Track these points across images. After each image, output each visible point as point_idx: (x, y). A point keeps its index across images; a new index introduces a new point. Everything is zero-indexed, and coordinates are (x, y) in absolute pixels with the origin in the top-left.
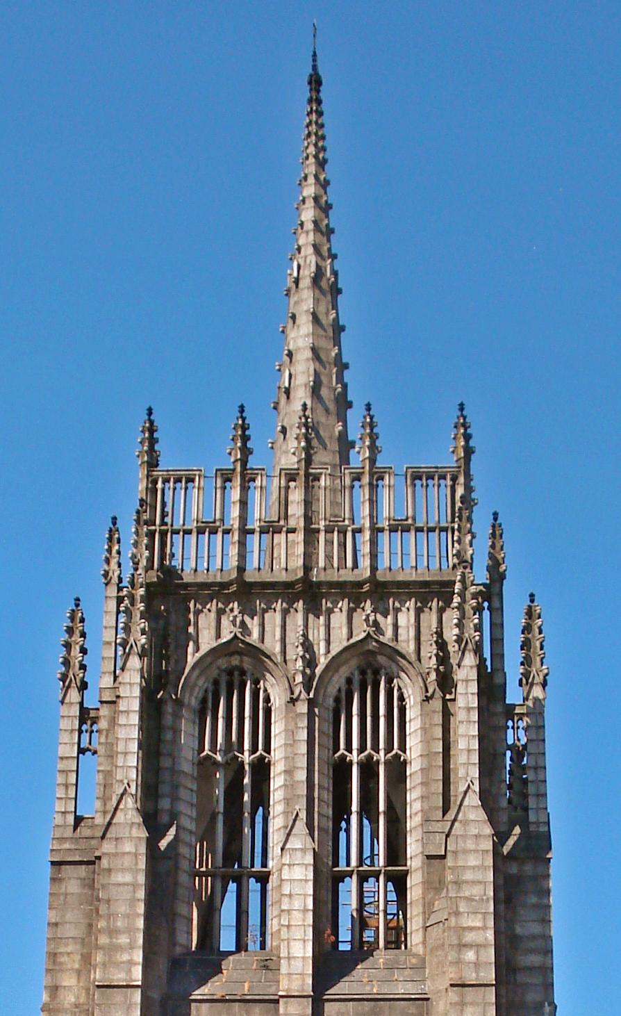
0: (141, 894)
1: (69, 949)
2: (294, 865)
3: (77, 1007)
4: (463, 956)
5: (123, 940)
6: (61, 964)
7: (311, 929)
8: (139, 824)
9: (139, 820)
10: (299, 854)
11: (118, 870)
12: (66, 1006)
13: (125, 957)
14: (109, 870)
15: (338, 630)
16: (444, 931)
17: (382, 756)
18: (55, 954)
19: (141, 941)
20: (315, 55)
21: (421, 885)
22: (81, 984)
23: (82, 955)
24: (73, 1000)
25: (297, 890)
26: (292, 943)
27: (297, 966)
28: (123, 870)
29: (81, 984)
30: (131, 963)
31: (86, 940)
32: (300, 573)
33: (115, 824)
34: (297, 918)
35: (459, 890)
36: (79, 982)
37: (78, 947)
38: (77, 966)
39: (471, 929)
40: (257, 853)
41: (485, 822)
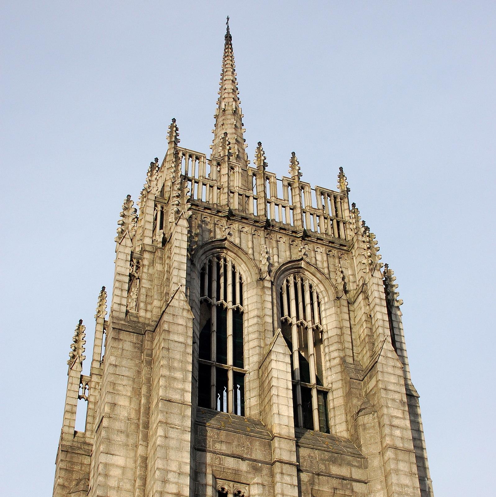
0: (190, 350)
1: (124, 383)
2: (279, 361)
3: (128, 420)
4: (393, 432)
5: (179, 375)
6: (117, 390)
7: (292, 400)
8: (188, 311)
9: (188, 307)
10: (282, 356)
11: (174, 333)
12: (121, 417)
13: (180, 386)
14: (169, 331)
15: (282, 252)
16: (374, 419)
17: (310, 325)
18: (115, 384)
19: (190, 378)
20: (228, 38)
21: (342, 398)
22: (132, 406)
23: (133, 388)
24: (126, 415)
25: (281, 376)
26: (280, 406)
27: (285, 421)
28: (178, 334)
29: (132, 406)
30: (184, 390)
31: (136, 380)
32: (136, 275)
33: (170, 306)
34: (283, 393)
35: (387, 394)
36: (130, 405)
37: (131, 383)
38: (129, 394)
39: (397, 417)
40: (294, 332)
41: (397, 360)
